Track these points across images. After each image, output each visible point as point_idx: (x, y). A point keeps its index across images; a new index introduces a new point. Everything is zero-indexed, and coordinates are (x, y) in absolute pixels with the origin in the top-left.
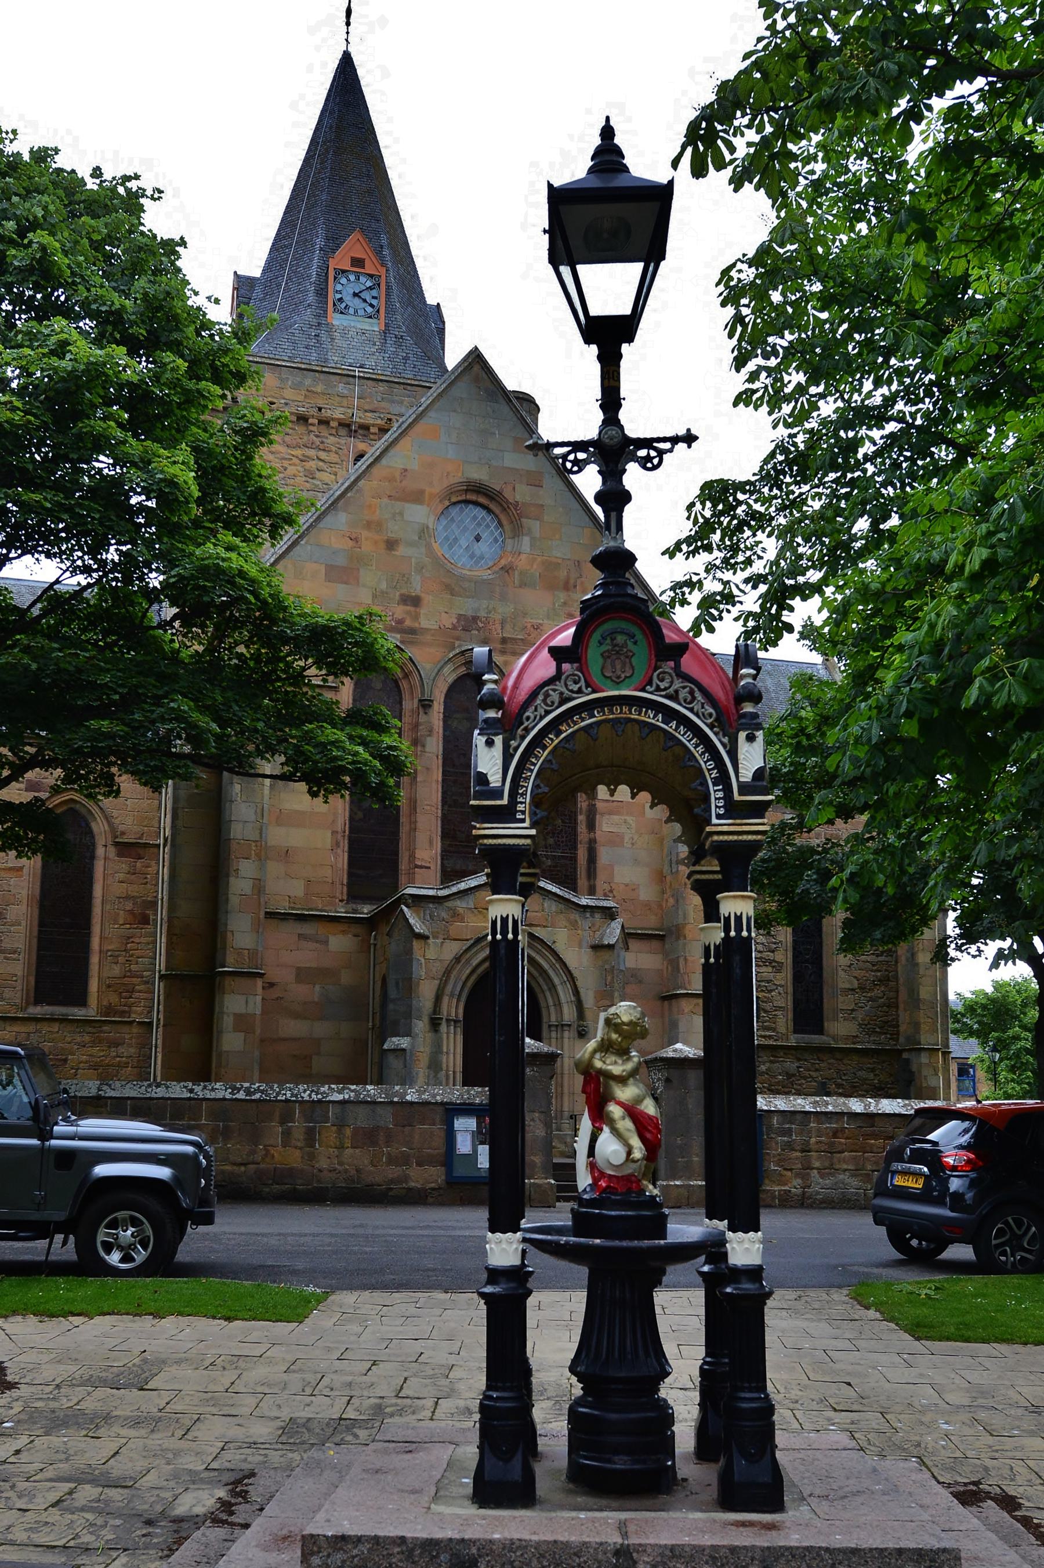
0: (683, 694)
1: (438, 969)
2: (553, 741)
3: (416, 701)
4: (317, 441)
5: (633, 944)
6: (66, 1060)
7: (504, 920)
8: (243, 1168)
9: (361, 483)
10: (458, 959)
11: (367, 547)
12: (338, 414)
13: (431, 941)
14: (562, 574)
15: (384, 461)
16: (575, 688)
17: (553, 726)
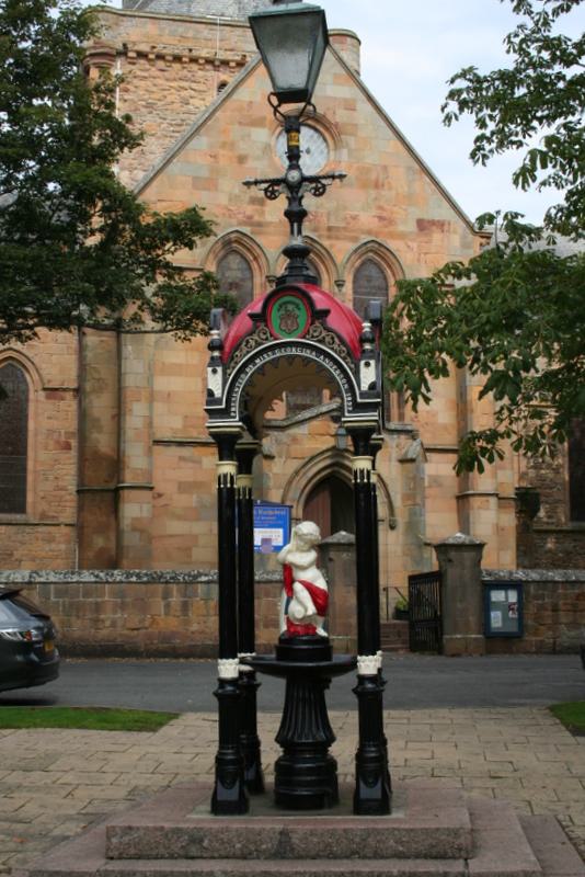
0: (327, 339)
1: (284, 481)
2: (251, 370)
3: (264, 278)
4: (189, 75)
5: (432, 456)
6: (12, 555)
7: (225, 476)
8: (136, 632)
9: (217, 114)
10: (297, 473)
11: (223, 162)
12: (204, 53)
13: (276, 460)
14: (373, 176)
15: (235, 97)
16: (264, 337)
17: (251, 360)
